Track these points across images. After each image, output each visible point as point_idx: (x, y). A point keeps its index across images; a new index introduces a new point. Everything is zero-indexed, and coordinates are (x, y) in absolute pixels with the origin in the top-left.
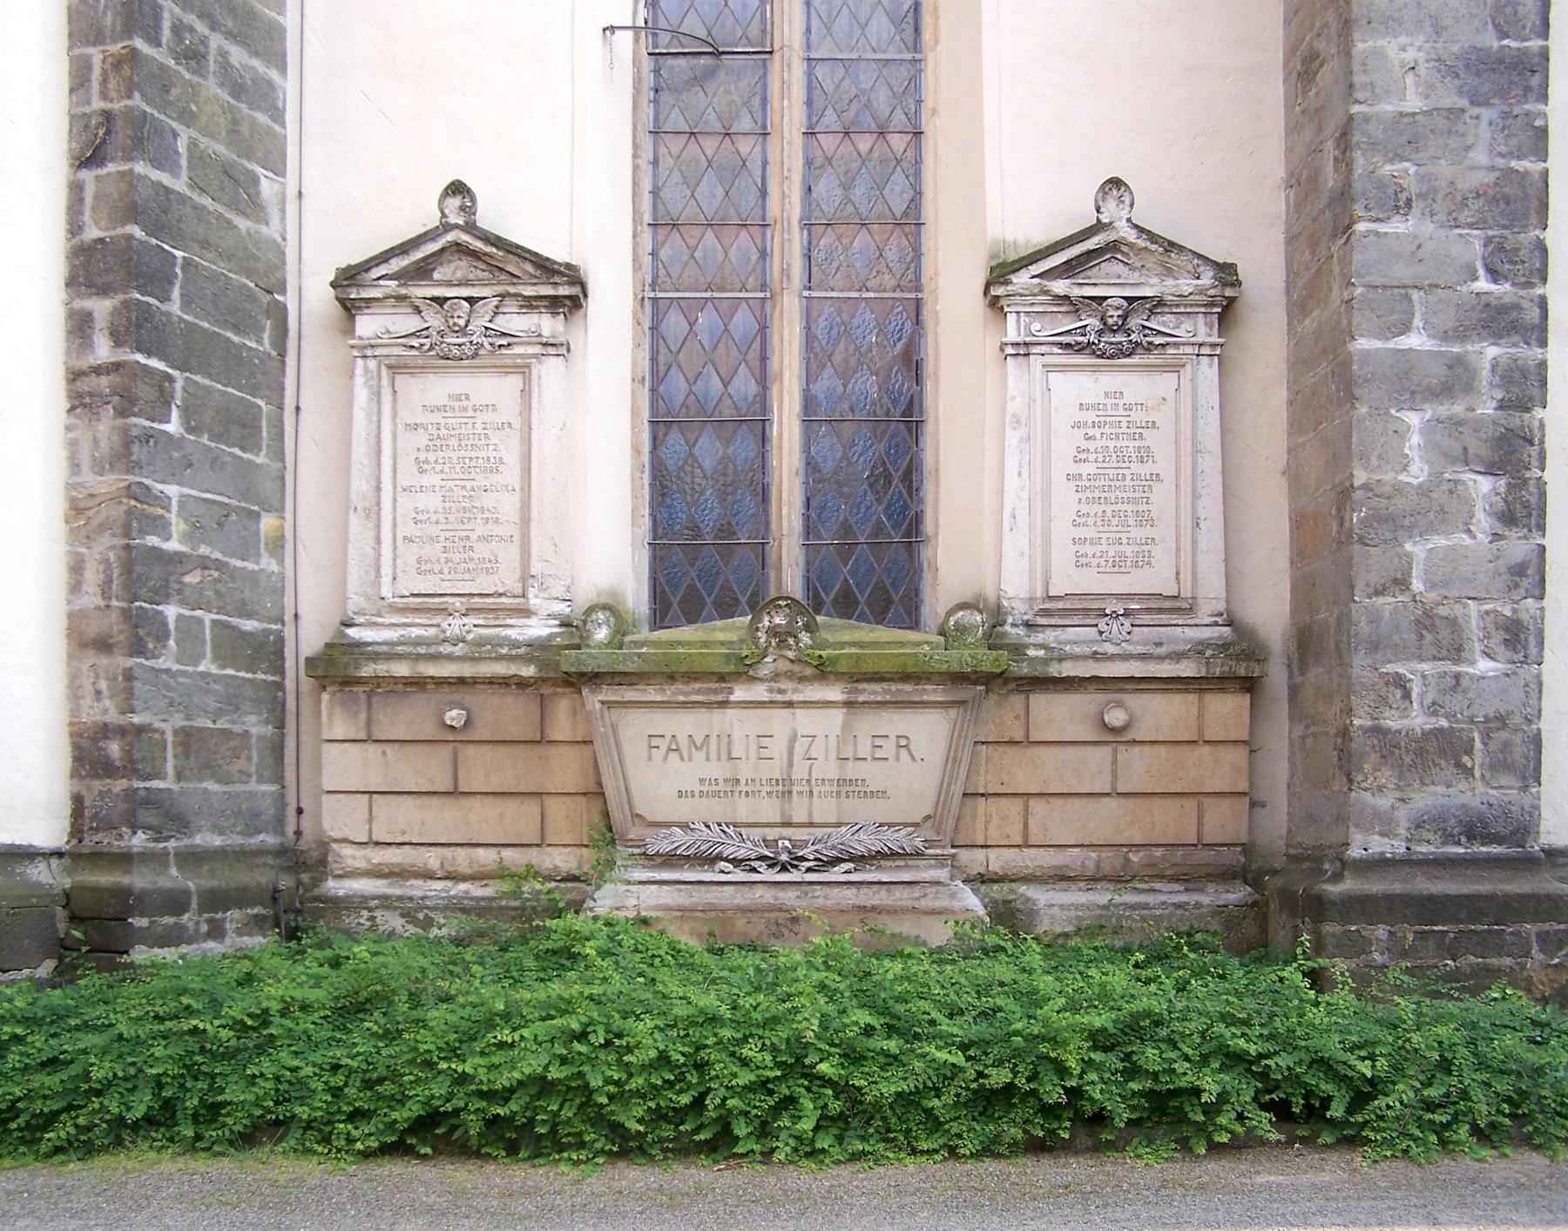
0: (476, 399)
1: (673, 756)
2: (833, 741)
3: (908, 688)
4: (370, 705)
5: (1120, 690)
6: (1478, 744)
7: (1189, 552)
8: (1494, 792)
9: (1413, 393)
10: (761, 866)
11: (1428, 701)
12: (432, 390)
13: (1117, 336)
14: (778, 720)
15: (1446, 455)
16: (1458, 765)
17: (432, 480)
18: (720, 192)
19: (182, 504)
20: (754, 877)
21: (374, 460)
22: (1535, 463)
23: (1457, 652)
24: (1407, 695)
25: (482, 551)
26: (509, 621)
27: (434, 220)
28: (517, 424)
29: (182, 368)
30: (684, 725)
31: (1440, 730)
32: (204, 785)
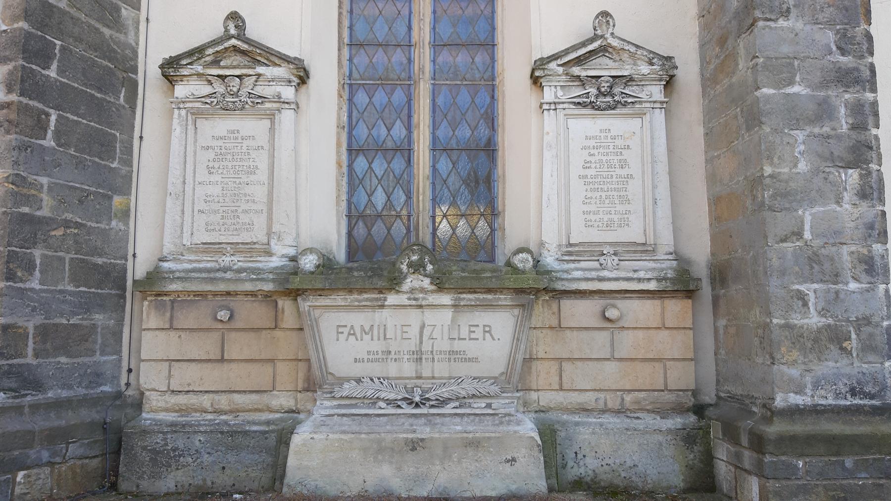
0: (243, 133)
1: (352, 338)
2: (446, 329)
3: (490, 297)
4: (172, 308)
5: (614, 298)
6: (854, 336)
7: (651, 219)
8: (866, 366)
9: (797, 120)
10: (404, 404)
11: (819, 308)
12: (219, 126)
13: (608, 97)
14: (414, 317)
15: (820, 156)
16: (842, 349)
17: (216, 178)
18: (387, 29)
19: (50, 189)
20: (399, 411)
21: (183, 166)
22: (875, 160)
23: (836, 277)
24: (805, 304)
25: (244, 218)
26: (259, 259)
27: (219, 31)
28: (266, 147)
29: (56, 108)
30: (358, 319)
31: (829, 325)
32: (58, 359)
